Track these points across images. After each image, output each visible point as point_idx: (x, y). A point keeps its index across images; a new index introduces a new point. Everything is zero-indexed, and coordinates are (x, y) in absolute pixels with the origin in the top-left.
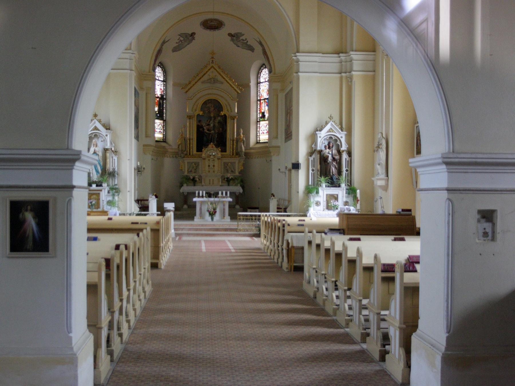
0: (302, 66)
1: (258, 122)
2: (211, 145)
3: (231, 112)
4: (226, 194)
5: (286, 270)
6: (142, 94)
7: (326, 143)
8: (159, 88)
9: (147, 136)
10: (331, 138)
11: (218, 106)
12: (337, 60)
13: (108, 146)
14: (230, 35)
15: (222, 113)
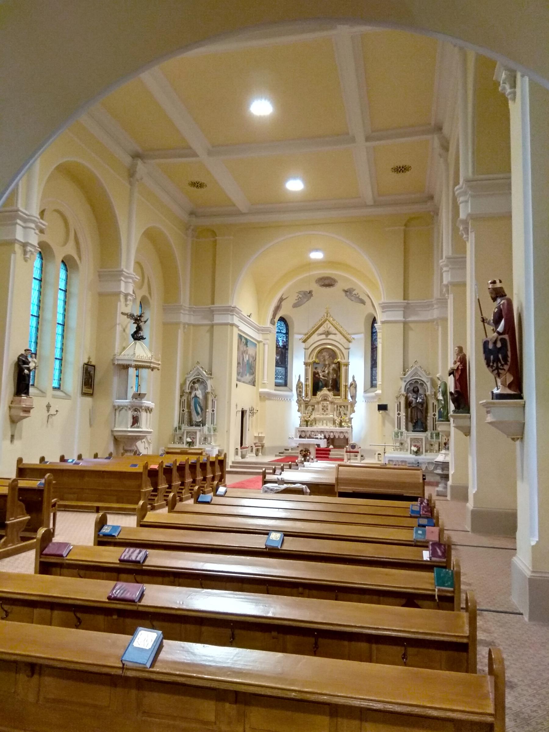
11: (333, 355)
15: (336, 361)
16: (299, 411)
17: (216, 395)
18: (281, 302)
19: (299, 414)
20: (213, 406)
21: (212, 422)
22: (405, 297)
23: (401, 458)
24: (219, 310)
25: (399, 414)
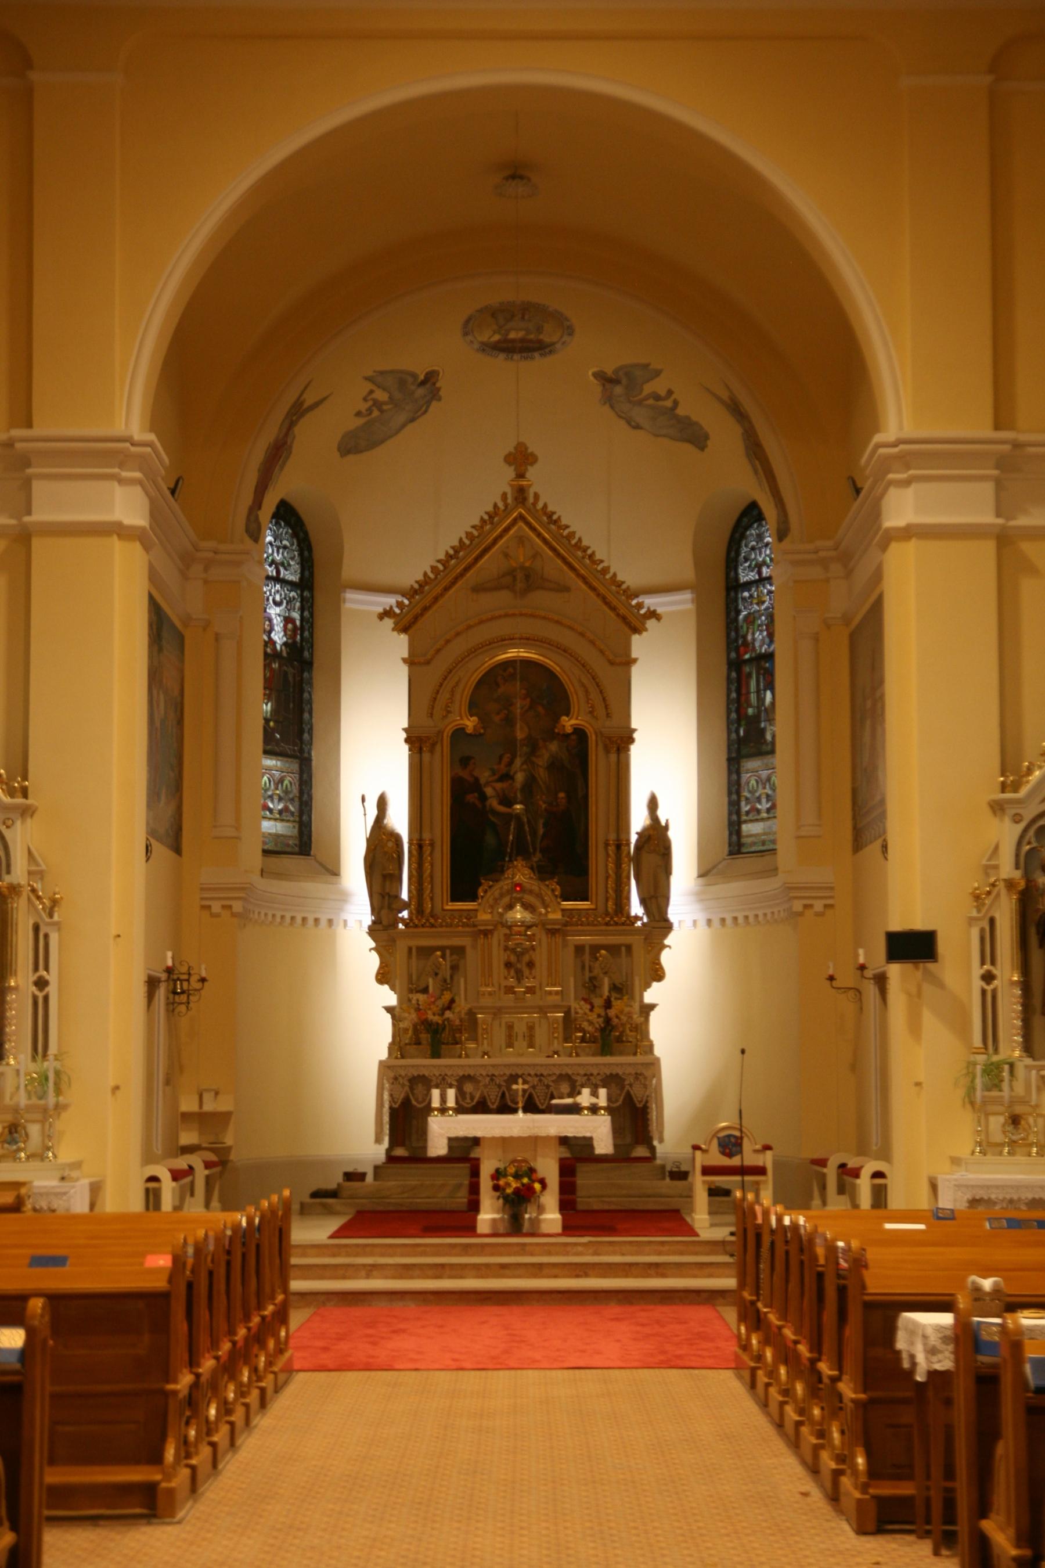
2: (520, 873)
3: (608, 715)
11: (547, 691)
15: (568, 723)
16: (382, 977)
17: (55, 902)
18: (292, 425)
19: (389, 997)
20: (41, 958)
21: (39, 1047)
22: (1003, 416)
23: (1028, 1187)
24: (905, 461)
25: (988, 978)
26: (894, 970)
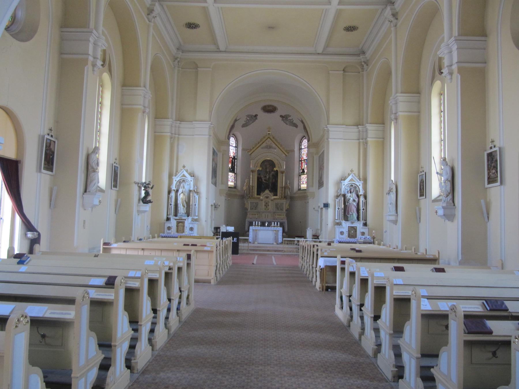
0: (331, 135)
1: (300, 176)
2: (267, 191)
4: (277, 224)
5: (318, 289)
6: (220, 155)
7: (349, 189)
8: (232, 152)
9: (222, 183)
10: (352, 185)
12: (357, 130)
13: (192, 189)
14: (281, 116)
15: (275, 169)
26: (324, 209)
